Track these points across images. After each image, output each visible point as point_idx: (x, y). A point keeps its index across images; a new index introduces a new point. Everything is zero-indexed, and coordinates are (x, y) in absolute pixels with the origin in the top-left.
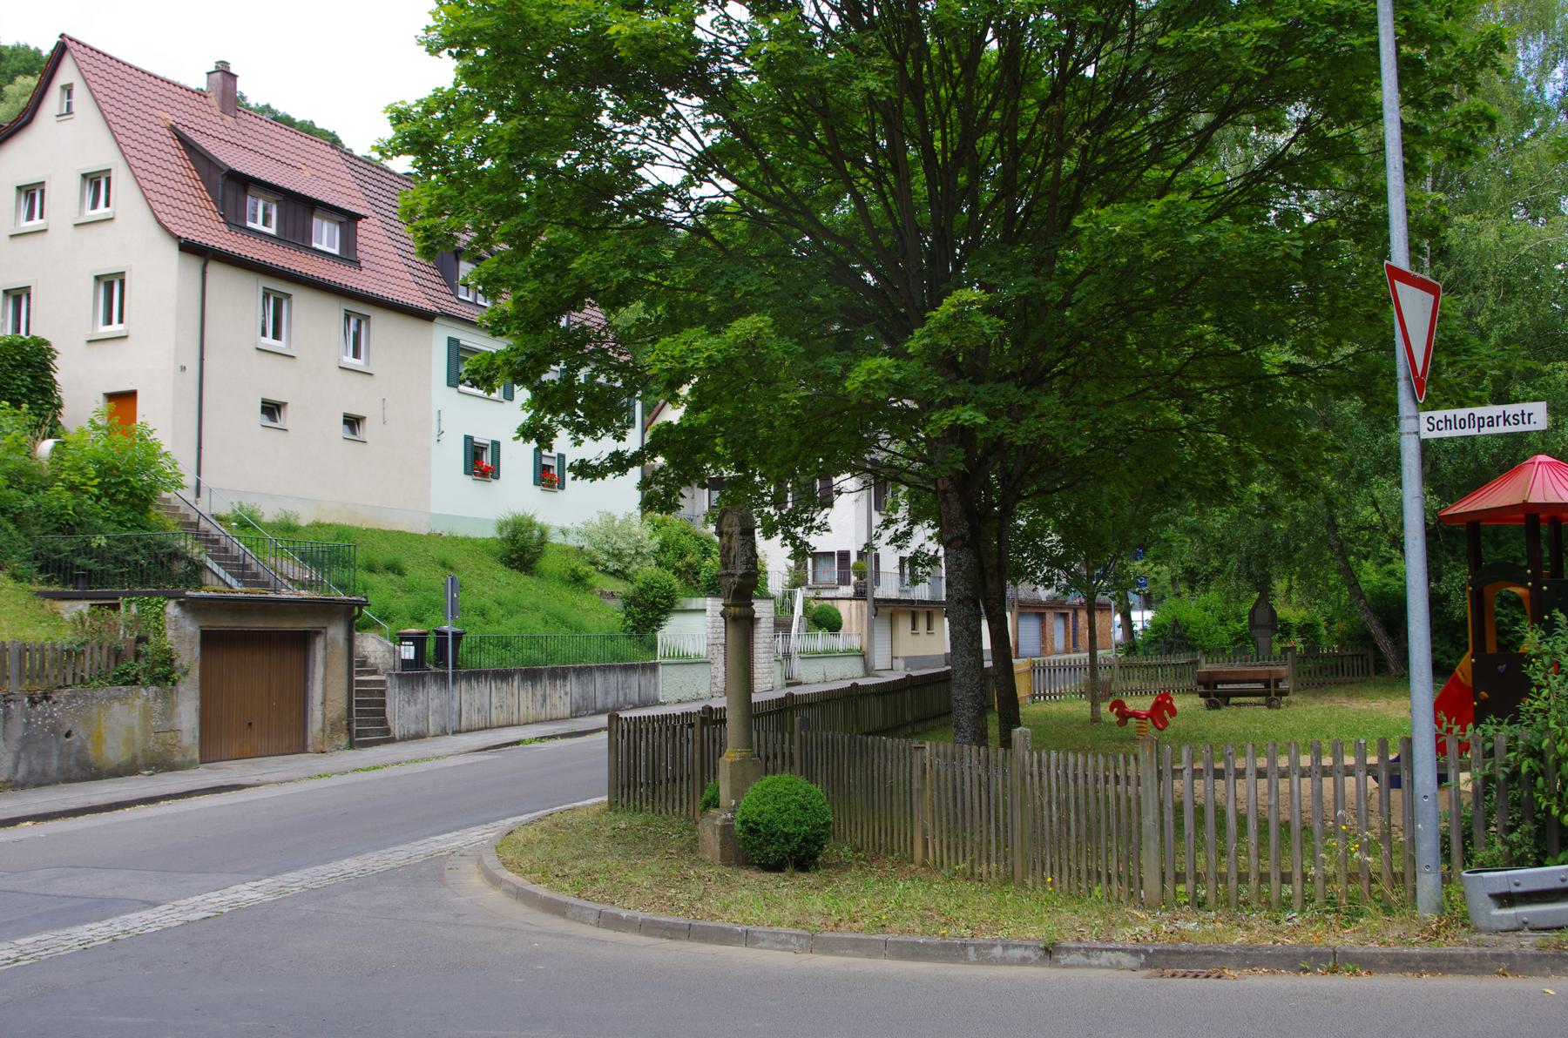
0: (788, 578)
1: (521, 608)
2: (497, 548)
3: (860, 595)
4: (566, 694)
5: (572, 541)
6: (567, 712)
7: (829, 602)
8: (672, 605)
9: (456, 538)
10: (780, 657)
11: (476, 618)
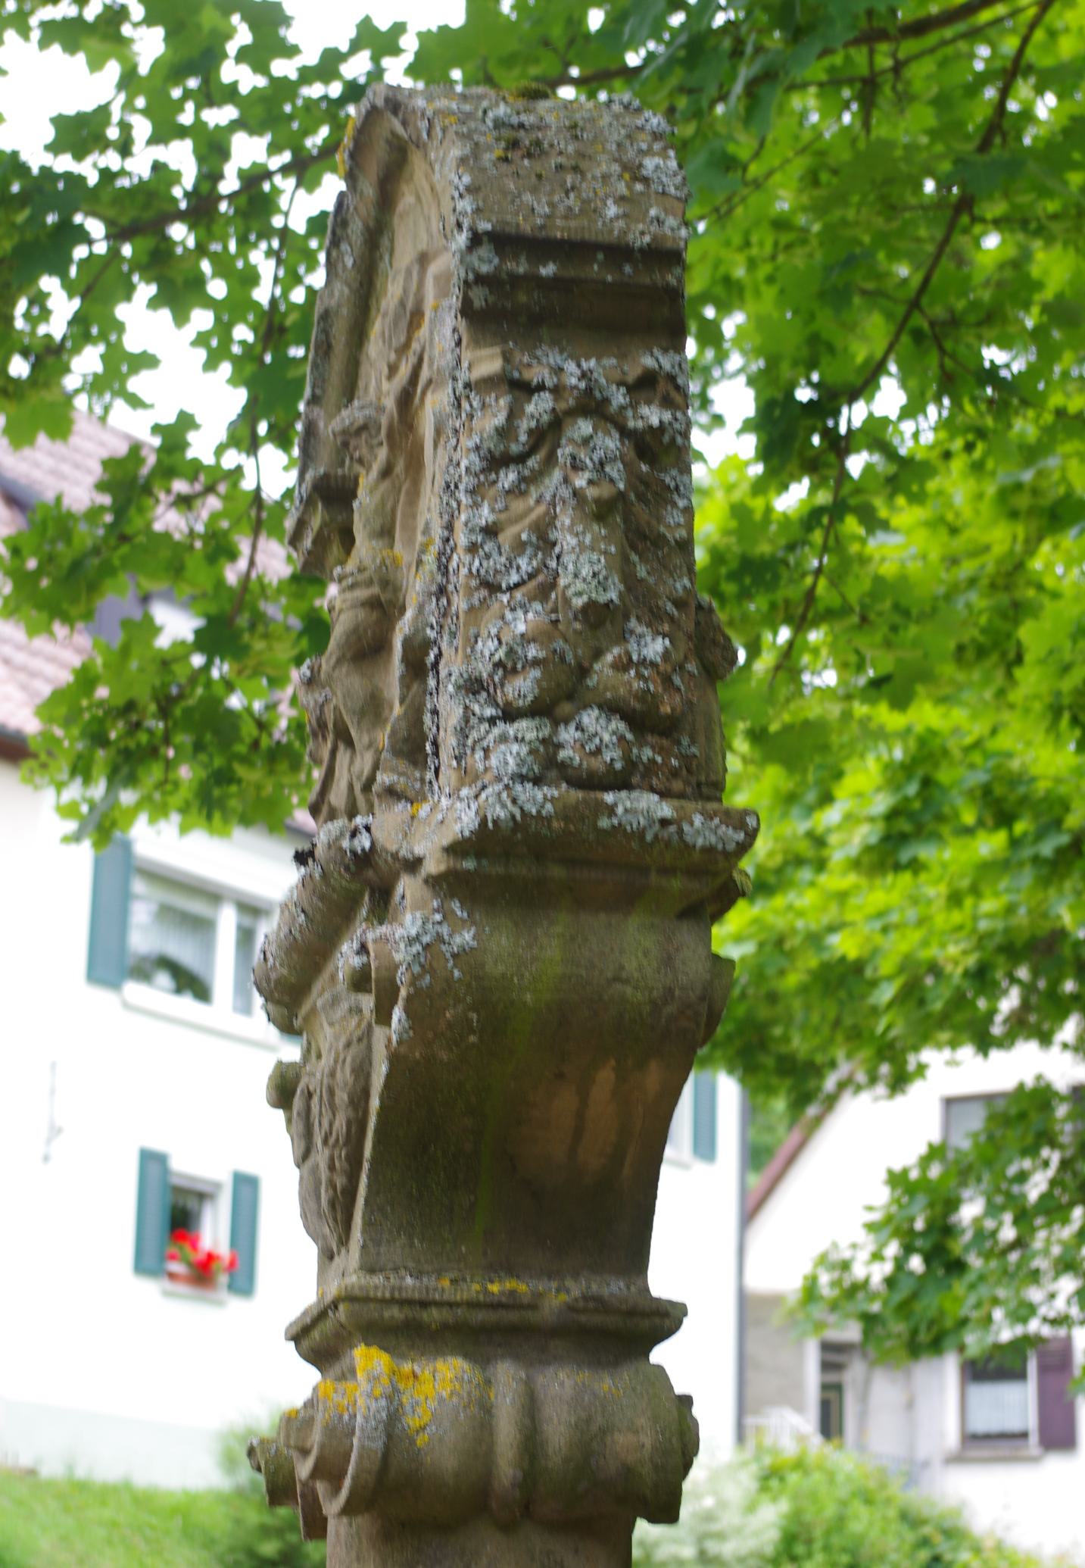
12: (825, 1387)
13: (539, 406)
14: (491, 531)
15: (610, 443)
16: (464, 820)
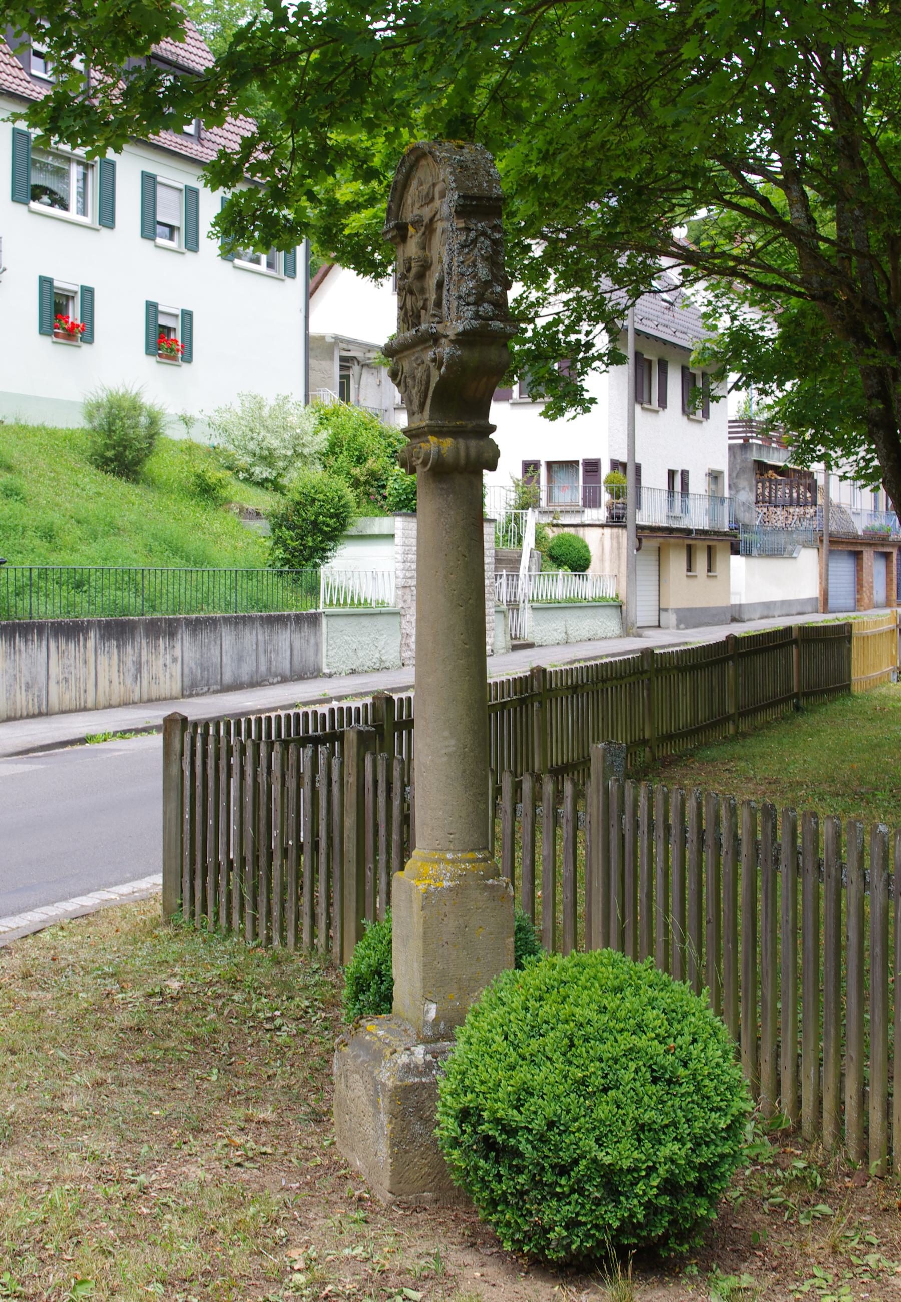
0: (513, 495)
1: (114, 529)
2: (86, 444)
3: (616, 520)
4: (175, 660)
5: (202, 437)
6: (176, 688)
7: (572, 531)
8: (343, 526)
9: (24, 428)
10: (504, 607)
11: (37, 542)
12: (341, 377)
13: (472, 234)
14: (462, 263)
15: (488, 242)
16: (460, 328)
